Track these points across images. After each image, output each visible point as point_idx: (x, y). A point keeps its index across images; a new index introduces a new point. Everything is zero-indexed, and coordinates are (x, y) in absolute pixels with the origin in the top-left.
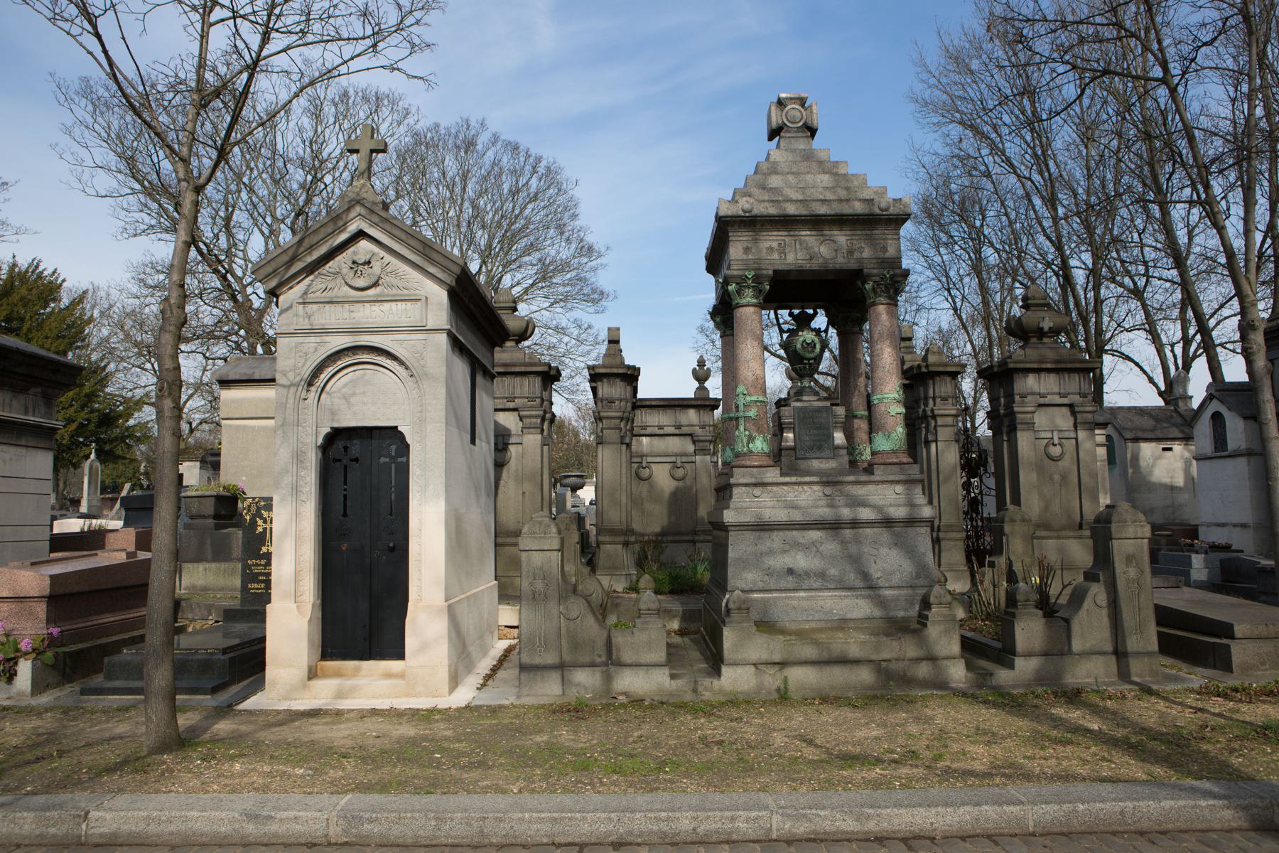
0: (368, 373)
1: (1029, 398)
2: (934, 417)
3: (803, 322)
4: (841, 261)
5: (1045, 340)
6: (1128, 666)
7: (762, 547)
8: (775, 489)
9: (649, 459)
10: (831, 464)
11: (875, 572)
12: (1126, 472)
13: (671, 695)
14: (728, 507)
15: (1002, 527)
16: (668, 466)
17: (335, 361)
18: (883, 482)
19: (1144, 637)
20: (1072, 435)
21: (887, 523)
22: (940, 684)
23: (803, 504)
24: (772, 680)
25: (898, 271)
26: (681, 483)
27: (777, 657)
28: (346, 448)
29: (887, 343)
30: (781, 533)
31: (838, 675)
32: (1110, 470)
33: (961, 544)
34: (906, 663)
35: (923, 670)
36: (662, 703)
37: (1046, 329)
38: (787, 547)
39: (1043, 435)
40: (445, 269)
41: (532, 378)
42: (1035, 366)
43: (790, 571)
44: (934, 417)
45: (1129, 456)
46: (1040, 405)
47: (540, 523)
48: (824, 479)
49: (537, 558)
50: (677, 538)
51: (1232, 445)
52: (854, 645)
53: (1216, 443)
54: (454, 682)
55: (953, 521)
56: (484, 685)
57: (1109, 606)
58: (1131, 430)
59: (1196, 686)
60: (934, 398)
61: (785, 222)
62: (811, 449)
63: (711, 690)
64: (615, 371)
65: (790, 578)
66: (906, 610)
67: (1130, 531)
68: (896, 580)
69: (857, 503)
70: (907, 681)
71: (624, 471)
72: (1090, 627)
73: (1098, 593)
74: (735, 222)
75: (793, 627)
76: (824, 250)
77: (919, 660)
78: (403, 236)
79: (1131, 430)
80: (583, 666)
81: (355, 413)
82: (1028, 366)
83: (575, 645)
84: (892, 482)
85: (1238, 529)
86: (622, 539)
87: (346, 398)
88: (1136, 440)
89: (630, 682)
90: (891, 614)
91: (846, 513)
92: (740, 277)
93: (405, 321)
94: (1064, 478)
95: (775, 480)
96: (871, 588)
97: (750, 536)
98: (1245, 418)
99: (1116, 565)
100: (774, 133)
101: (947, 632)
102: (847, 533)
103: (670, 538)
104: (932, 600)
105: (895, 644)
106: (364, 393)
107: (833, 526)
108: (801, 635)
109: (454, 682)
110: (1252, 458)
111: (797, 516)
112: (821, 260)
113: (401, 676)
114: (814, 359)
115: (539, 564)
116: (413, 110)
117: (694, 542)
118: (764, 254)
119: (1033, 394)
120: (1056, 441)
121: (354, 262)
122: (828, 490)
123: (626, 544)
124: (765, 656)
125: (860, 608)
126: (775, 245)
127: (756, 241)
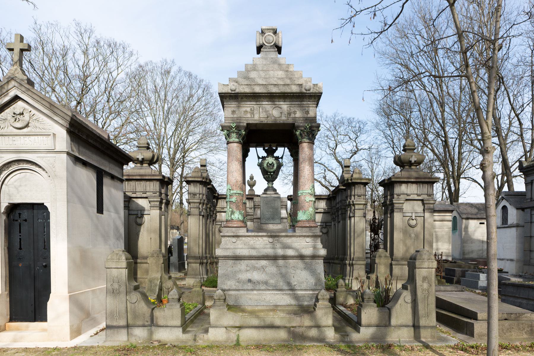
0: (28, 174)
1: (402, 196)
2: (354, 205)
3: (270, 152)
4: (284, 119)
5: (413, 167)
6: (419, 333)
7: (236, 269)
8: (243, 238)
10: (279, 227)
11: (294, 282)
12: (461, 234)
13: (182, 342)
15: (375, 260)
17: (8, 168)
18: (300, 236)
19: (428, 317)
20: (422, 215)
21: (301, 257)
22: (321, 340)
23: (258, 246)
24: (233, 335)
25: (314, 124)
27: (237, 324)
28: (20, 214)
29: (307, 163)
30: (246, 261)
31: (269, 334)
32: (453, 232)
33: (364, 267)
34: (304, 328)
35: (313, 333)
36: (175, 346)
37: (413, 161)
38: (248, 268)
39: (407, 215)
40: (63, 118)
41: (155, 182)
42: (406, 180)
43: (250, 281)
44: (354, 205)
45: (463, 226)
46: (407, 200)
47: (117, 254)
48: (269, 234)
51: (510, 222)
52: (278, 319)
53: (503, 221)
54: (76, 332)
55: (361, 256)
57: (412, 302)
58: (466, 214)
59: (452, 344)
60: (354, 196)
61: (255, 97)
62: (269, 219)
64: (196, 179)
65: (249, 284)
66: (309, 301)
67: (426, 265)
68: (304, 286)
69: (286, 247)
70: (303, 338)
71: (201, 228)
72: (401, 312)
73: (407, 296)
74: (227, 96)
75: (249, 308)
76: (275, 113)
77: (311, 327)
78: (39, 99)
79: (466, 214)
80: (139, 326)
81: (21, 196)
82: (402, 180)
84: (305, 236)
85: (509, 262)
86: (199, 261)
87: (16, 188)
88: (467, 219)
89: (162, 335)
90: (300, 303)
91: (280, 252)
92: (229, 127)
93: (43, 147)
94: (417, 236)
95: (243, 234)
96: (292, 290)
97: (230, 262)
98: (517, 209)
99: (417, 282)
100: (259, 49)
101: (326, 314)
102: (281, 262)
104: (319, 297)
105: (298, 319)
106: (26, 185)
107: (274, 258)
108: (253, 313)
110: (519, 228)
111: (254, 253)
112: (273, 118)
113: (44, 330)
114: (274, 172)
115: (116, 275)
116: (134, 52)
118: (243, 115)
119: (403, 194)
120: (414, 218)
121: (14, 114)
122: (271, 240)
124: (231, 323)
125: (285, 299)
126: (248, 109)
127: (239, 107)
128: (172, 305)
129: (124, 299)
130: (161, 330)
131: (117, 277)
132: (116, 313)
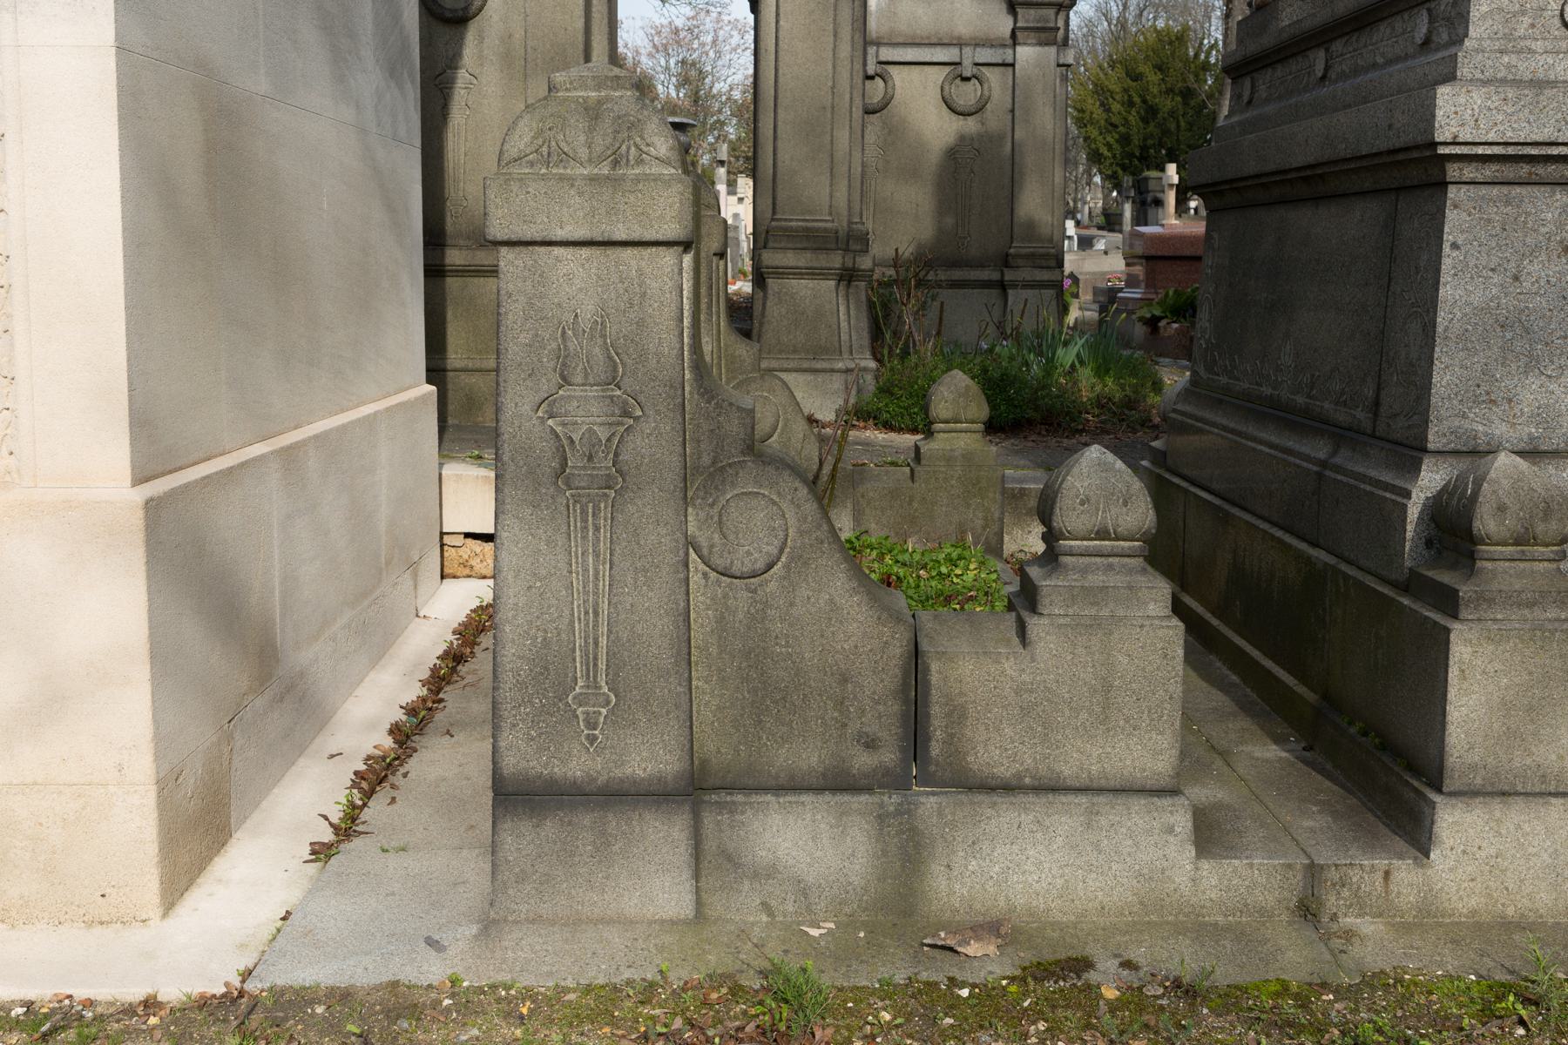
9: (887, 54)
13: (1199, 928)
14: (1450, 77)
16: (939, 74)
26: (971, 125)
47: (593, 113)
49: (574, 282)
50: (957, 274)
54: (197, 828)
56: (348, 827)
63: (1384, 910)
80: (792, 786)
83: (766, 688)
86: (836, 260)
89: (1029, 869)
103: (943, 275)
109: (197, 828)
115: (588, 310)
117: (1002, 286)
123: (847, 277)
128: (1095, 595)
129: (659, 538)
130: (1004, 817)
131: (599, 328)
132: (591, 663)
